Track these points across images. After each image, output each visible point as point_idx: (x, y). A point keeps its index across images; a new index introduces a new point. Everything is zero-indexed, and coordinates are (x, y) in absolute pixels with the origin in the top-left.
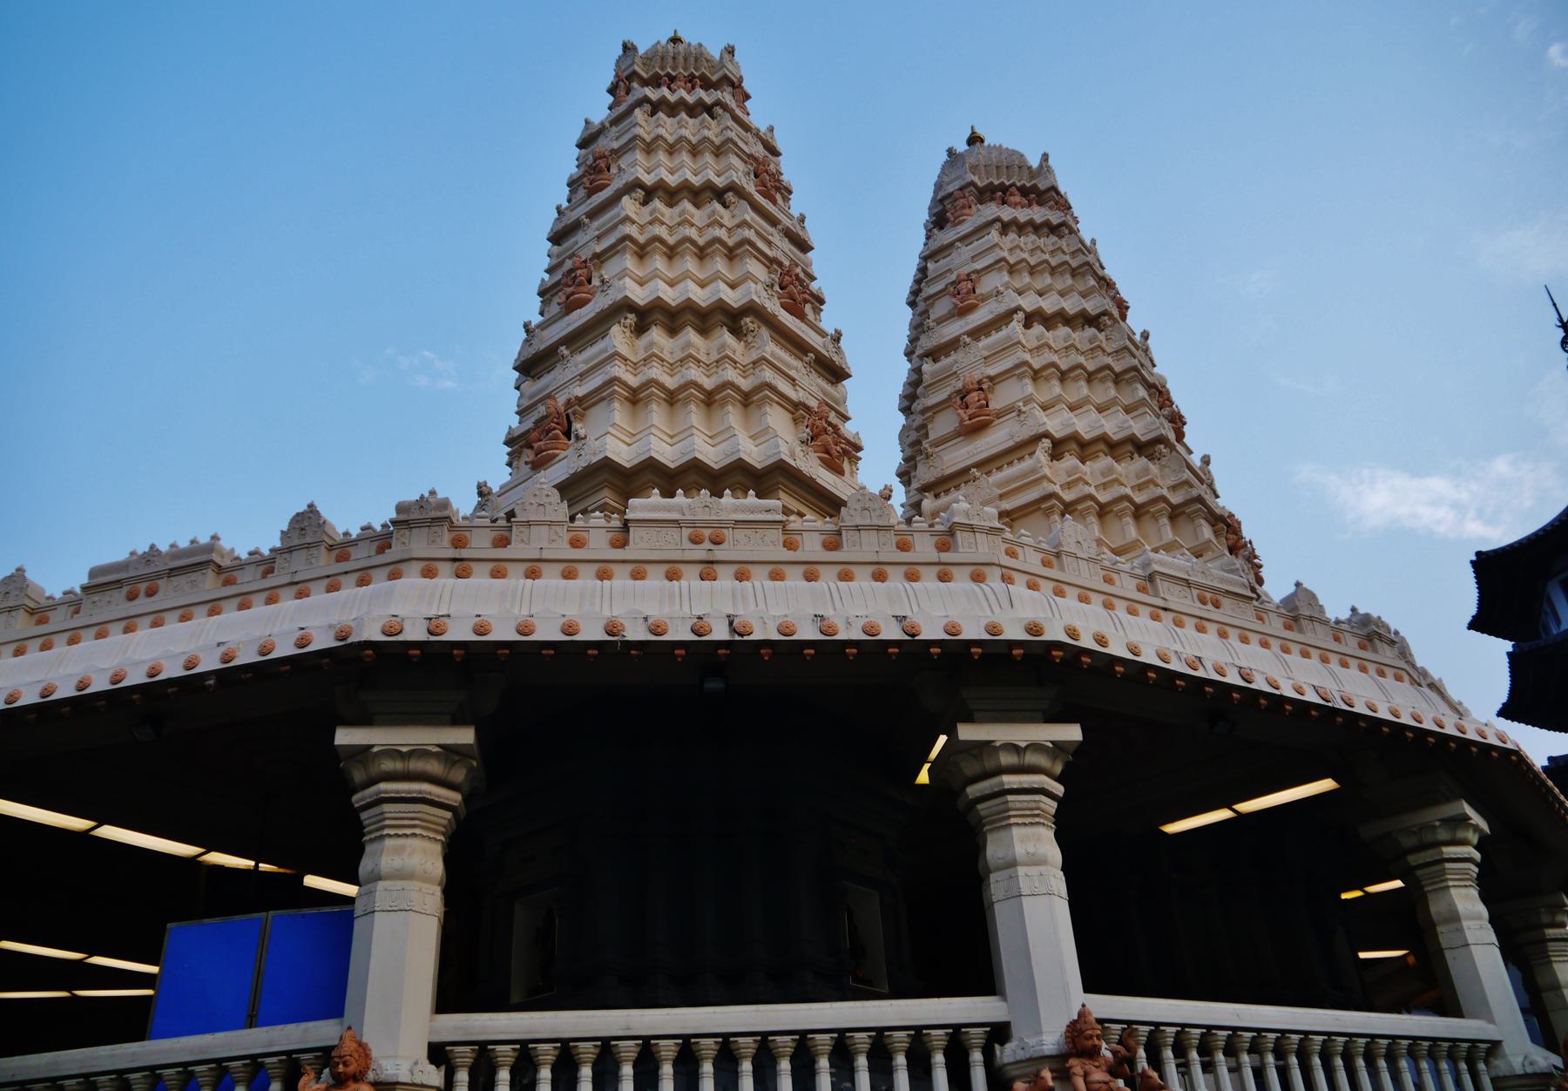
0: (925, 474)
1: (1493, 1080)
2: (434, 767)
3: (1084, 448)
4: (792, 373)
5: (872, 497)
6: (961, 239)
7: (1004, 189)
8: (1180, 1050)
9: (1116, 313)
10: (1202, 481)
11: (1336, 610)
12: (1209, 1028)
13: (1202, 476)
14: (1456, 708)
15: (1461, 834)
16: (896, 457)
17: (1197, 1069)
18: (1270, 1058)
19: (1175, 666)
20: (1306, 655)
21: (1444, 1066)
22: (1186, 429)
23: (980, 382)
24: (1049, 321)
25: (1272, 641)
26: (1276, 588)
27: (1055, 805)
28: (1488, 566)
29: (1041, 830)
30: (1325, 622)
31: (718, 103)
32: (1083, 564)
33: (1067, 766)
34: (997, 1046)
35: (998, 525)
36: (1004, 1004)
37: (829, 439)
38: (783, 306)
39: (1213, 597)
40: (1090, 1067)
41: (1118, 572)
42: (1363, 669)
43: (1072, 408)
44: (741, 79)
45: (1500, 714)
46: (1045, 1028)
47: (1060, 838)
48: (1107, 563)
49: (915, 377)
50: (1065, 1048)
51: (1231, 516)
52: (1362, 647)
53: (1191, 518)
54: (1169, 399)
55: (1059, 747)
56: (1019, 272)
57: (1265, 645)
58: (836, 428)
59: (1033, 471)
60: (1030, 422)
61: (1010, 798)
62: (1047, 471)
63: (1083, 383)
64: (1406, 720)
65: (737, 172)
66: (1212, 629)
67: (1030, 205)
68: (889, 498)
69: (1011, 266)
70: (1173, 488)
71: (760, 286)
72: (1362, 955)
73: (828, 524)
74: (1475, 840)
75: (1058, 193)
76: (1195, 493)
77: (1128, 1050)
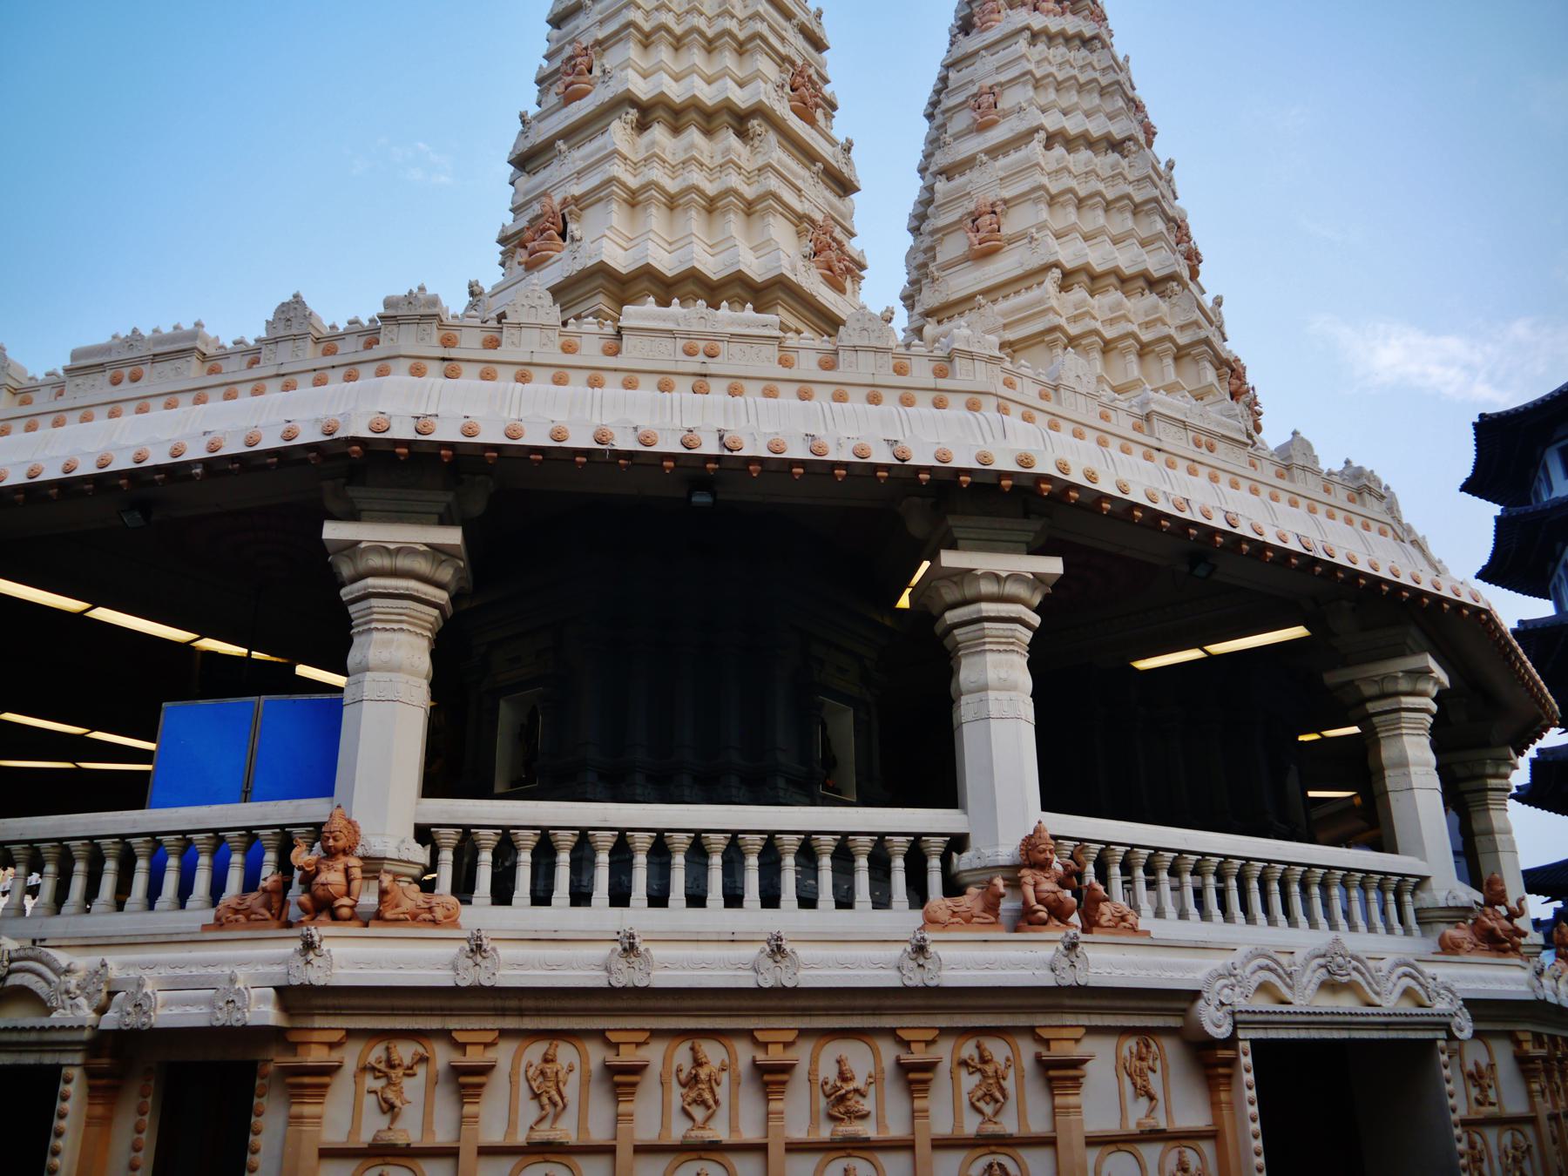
3: (1095, 280)
4: (799, 183)
5: (872, 318)
6: (986, 48)
8: (1127, 868)
9: (1142, 138)
10: (1211, 323)
11: (1330, 461)
13: (1212, 317)
14: (1435, 566)
15: (1421, 686)
16: (900, 279)
18: (1211, 880)
19: (1163, 506)
20: (1293, 504)
21: (1373, 895)
22: (1201, 267)
23: (993, 205)
26: (1273, 436)
27: (1030, 634)
28: (1490, 430)
29: (1015, 657)
30: (1318, 473)
32: (1081, 399)
33: (1046, 597)
35: (997, 353)
37: (833, 255)
38: (793, 109)
39: (1208, 440)
40: (1040, 876)
41: (1115, 409)
42: (1349, 522)
43: (1086, 238)
45: (1479, 576)
46: (1001, 840)
48: (1104, 400)
49: (927, 195)
50: (1018, 860)
51: (1237, 360)
52: (1351, 500)
54: (1187, 235)
55: (1039, 579)
58: (840, 244)
59: (1040, 301)
61: (987, 625)
62: (1054, 303)
68: (890, 320)
69: (1037, 81)
70: (1182, 328)
71: (770, 87)
72: (1311, 794)
73: (824, 343)
74: (1434, 693)
76: (1202, 334)
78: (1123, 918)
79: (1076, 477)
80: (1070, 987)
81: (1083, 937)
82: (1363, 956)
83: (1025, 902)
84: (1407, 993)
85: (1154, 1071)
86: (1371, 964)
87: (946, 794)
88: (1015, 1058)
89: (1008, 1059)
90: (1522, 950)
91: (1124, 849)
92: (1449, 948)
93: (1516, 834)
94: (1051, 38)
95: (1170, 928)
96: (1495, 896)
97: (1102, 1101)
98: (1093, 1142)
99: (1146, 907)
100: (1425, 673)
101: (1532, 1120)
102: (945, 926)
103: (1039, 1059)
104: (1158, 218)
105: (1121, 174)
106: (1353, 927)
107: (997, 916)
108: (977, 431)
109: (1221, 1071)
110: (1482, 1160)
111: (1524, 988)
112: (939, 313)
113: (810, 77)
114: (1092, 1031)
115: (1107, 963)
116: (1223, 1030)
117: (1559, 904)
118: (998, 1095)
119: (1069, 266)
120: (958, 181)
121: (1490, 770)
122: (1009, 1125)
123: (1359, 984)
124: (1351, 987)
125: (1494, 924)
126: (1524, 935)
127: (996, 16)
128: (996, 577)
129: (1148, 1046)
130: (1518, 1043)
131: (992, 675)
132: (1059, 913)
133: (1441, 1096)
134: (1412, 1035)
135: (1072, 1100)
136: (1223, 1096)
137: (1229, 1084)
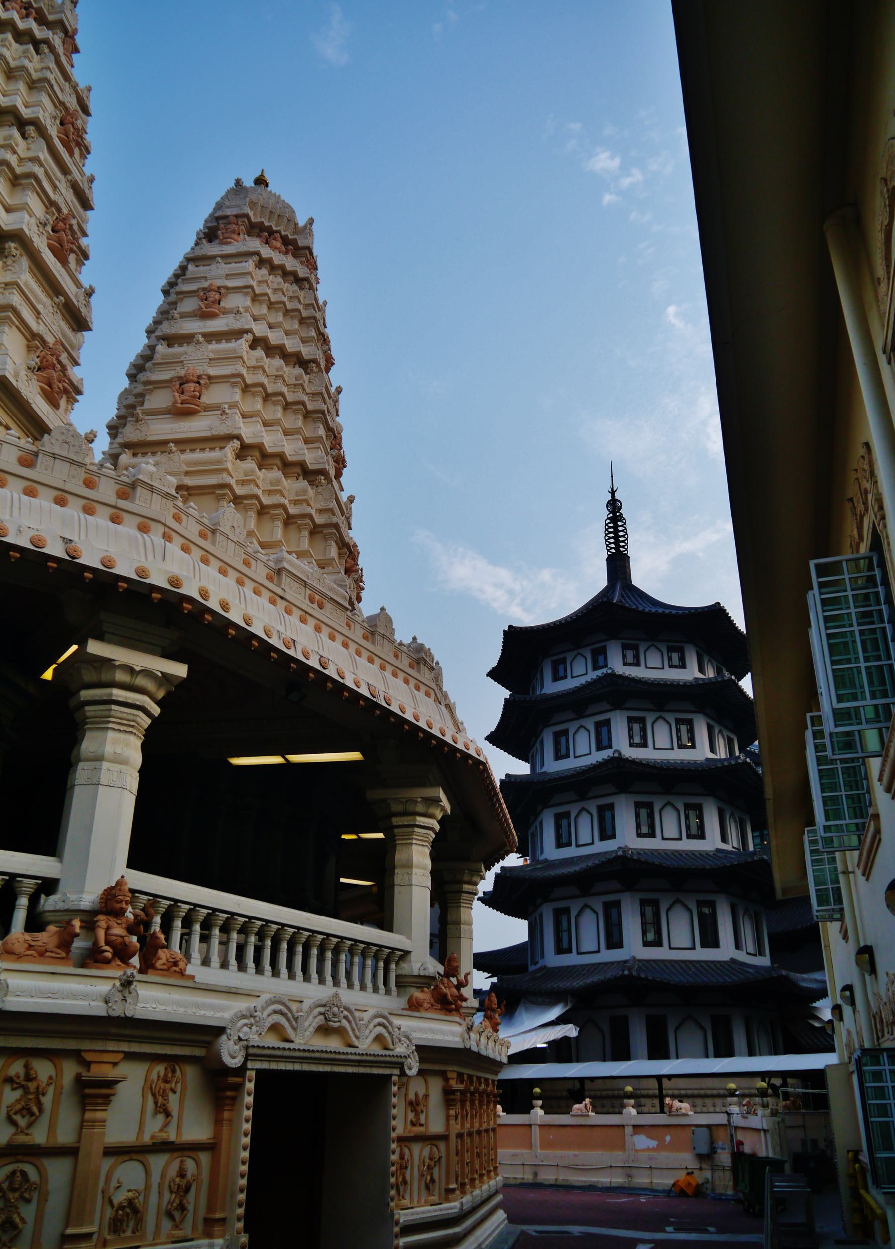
0: (130, 433)
1: (397, 976)
2: (150, 685)
3: (265, 458)
4: (40, 307)
5: (75, 435)
6: (224, 257)
7: (271, 232)
8: (188, 923)
9: (323, 364)
10: (342, 514)
11: (402, 635)
12: (215, 910)
13: (344, 510)
14: (458, 727)
15: (432, 810)
16: (111, 412)
17: (196, 938)
18: (252, 939)
19: (275, 641)
20: (371, 661)
21: (369, 962)
22: (344, 471)
23: (199, 377)
24: (271, 350)
25: (350, 643)
26: (368, 608)
27: (149, 721)
28: (514, 637)
29: (132, 738)
30: (392, 642)
31: (46, 41)
32: (231, 545)
33: (168, 694)
34: (43, 896)
35: (173, 493)
36: (58, 865)
37: (55, 375)
38: (50, 247)
39: (320, 599)
40: (113, 922)
41: (256, 559)
42: (406, 682)
43: (265, 424)
44: (75, 31)
45: (487, 738)
46: (87, 888)
47: (145, 748)
48: (249, 550)
49: (148, 352)
50: (98, 906)
51: (355, 546)
52: (411, 666)
53: (326, 538)
54: (340, 445)
55: (166, 678)
56: (260, 302)
57: (345, 645)
58: (64, 368)
59: (219, 462)
60: (229, 423)
61: (114, 707)
62: (229, 466)
63: (280, 408)
64: (422, 724)
65: (44, 111)
66: (312, 622)
67: (286, 253)
68: (92, 441)
69: (255, 295)
70: (320, 511)
71: (33, 221)
72: (342, 880)
73: (26, 443)
74: (439, 817)
75: (311, 254)
76: (334, 520)
77: (147, 915)
78: (175, 964)
79: (213, 604)
80: (119, 1018)
81: (139, 977)
82: (352, 1008)
83: (96, 943)
84: (379, 1038)
85: (174, 1092)
86: (357, 1014)
87: (47, 842)
88: (55, 1076)
89: (50, 1078)
90: (462, 1011)
91: (188, 907)
92: (414, 1006)
93: (474, 927)
94: (273, 268)
95: (213, 975)
96: (452, 970)
97: (126, 1117)
98: (112, 1151)
99: (196, 956)
100: (436, 801)
101: (445, 1138)
102: (19, 957)
103: (78, 1079)
104: (321, 426)
105: (302, 385)
106: (350, 985)
107: (68, 952)
108: (142, 551)
109: (229, 1094)
110: (406, 1168)
111: (458, 1039)
112: (139, 448)
113: (71, 226)
114: (130, 1056)
115: (155, 1000)
116: (236, 1060)
117: (495, 980)
118: (35, 1110)
119: (247, 441)
120: (176, 350)
121: (466, 878)
122: (39, 1136)
123: (345, 1029)
124: (340, 1032)
125: (447, 991)
126: (466, 1000)
127: (235, 236)
128: (130, 670)
129: (174, 1071)
130: (447, 1080)
131: (109, 749)
132: (122, 954)
133: (387, 1118)
134: (375, 1071)
135: (99, 1115)
136: (226, 1115)
137: (233, 1105)
